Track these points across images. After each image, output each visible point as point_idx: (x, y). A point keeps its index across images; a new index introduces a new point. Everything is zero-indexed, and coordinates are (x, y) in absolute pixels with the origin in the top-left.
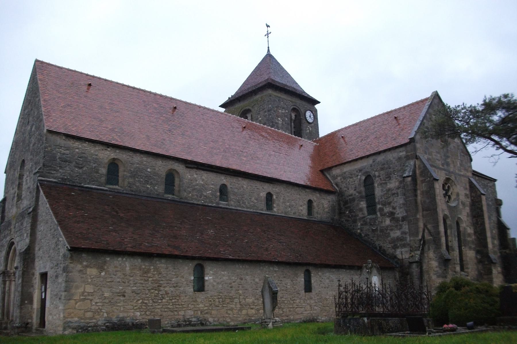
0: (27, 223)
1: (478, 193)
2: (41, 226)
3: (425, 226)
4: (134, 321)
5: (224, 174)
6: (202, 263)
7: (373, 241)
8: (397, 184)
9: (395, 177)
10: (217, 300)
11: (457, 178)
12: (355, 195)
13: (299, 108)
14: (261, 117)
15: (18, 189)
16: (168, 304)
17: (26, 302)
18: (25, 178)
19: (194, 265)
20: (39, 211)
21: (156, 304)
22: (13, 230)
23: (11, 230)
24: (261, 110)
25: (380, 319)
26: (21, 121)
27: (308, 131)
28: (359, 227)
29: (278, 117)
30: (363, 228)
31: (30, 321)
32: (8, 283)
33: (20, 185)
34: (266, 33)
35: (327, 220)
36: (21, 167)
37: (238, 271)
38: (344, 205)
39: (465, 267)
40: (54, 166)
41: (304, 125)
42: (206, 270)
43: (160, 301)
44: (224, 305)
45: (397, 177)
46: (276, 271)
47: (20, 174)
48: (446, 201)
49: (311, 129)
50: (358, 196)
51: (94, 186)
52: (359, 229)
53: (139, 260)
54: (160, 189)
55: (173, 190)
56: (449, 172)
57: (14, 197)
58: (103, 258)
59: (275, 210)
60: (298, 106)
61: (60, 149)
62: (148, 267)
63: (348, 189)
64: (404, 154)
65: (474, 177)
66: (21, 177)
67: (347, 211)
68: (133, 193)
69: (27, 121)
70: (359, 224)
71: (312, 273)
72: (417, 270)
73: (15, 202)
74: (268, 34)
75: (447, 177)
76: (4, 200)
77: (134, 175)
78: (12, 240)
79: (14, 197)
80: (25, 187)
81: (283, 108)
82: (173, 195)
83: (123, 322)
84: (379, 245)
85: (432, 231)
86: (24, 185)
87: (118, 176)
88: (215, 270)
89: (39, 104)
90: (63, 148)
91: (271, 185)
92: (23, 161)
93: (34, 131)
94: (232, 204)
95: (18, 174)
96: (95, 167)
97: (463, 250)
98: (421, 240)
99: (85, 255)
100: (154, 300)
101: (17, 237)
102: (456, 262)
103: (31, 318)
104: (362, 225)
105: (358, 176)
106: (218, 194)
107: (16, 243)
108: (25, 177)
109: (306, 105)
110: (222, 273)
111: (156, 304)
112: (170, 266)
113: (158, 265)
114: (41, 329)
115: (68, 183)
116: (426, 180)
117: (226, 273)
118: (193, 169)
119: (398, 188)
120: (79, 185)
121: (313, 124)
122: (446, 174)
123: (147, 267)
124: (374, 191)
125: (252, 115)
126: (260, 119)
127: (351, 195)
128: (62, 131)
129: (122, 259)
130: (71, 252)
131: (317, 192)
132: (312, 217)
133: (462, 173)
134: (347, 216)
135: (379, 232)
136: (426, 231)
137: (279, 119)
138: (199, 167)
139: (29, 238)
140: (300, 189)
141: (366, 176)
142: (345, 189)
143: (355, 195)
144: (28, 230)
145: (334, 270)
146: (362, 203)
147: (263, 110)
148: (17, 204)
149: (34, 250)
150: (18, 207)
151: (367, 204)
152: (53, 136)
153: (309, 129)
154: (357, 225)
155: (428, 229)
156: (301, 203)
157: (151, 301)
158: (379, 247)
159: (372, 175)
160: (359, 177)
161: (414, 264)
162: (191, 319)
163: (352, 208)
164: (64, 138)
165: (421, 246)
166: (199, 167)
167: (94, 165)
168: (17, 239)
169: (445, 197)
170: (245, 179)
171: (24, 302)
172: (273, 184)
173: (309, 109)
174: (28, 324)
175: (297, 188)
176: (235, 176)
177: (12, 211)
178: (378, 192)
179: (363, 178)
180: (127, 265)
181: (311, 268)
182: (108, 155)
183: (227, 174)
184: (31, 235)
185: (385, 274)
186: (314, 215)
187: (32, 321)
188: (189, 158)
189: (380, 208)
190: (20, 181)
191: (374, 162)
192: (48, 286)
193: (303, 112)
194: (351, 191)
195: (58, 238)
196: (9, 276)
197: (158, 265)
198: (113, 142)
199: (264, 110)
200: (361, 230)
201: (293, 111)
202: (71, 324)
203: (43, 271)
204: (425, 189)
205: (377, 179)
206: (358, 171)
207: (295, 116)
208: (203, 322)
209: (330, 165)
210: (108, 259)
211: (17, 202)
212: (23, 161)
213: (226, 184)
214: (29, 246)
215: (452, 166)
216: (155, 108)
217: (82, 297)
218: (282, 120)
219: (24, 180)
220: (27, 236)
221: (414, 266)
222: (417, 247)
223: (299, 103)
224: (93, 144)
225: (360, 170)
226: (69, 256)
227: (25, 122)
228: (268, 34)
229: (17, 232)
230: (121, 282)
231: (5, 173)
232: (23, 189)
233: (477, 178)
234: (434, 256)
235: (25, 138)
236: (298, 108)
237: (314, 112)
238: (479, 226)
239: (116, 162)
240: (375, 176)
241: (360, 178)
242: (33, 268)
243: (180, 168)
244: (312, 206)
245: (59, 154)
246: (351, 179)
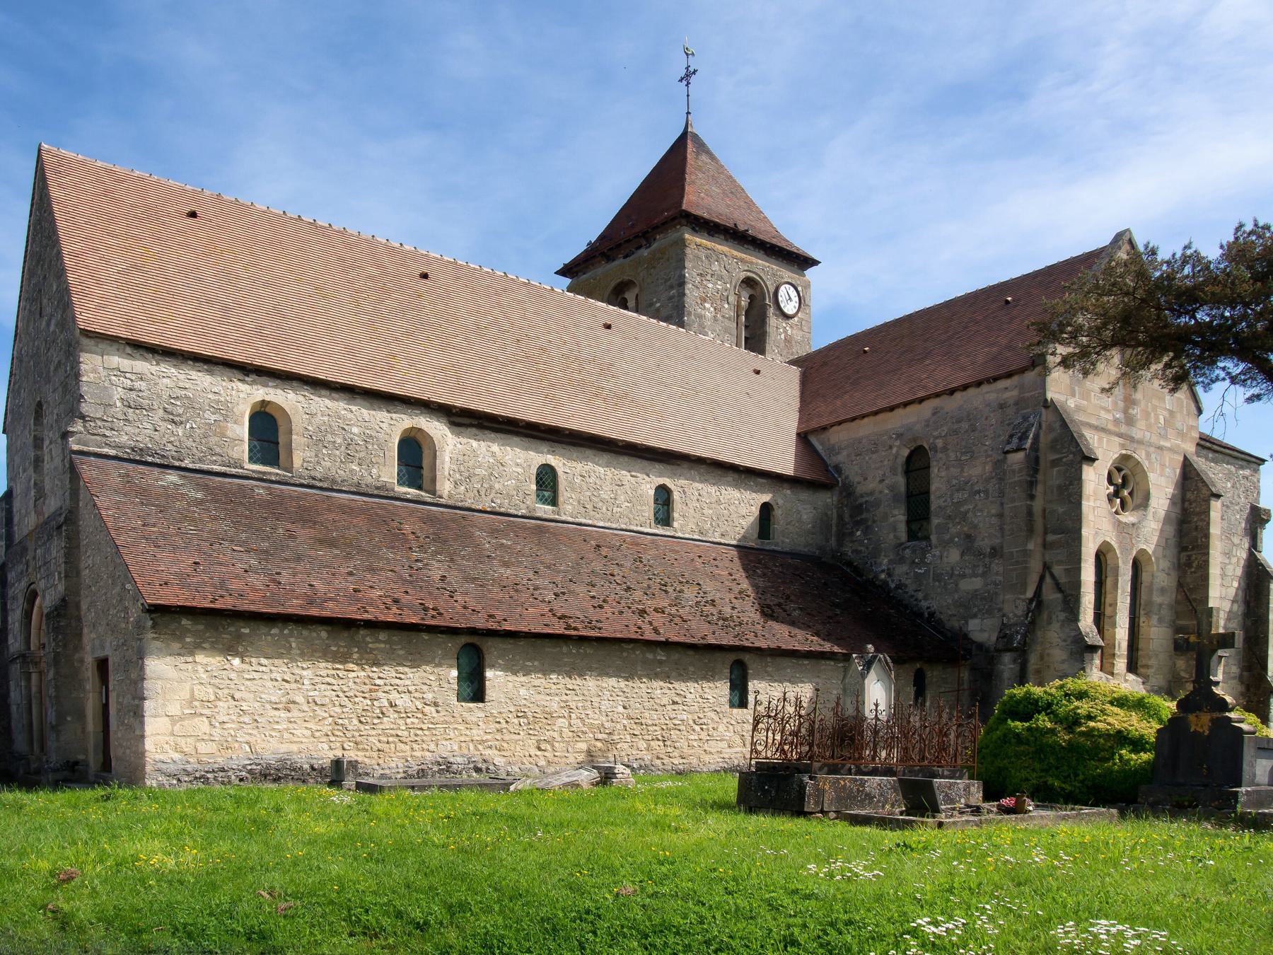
0: (56, 549)
1: (1204, 491)
2: (89, 556)
3: (1047, 567)
4: (314, 761)
5: (548, 440)
6: (478, 643)
7: (916, 600)
8: (988, 468)
9: (986, 451)
10: (516, 721)
11: (1153, 456)
12: (881, 492)
13: (761, 278)
14: (659, 300)
15: (35, 472)
16: (395, 726)
17: (69, 719)
18: (47, 448)
19: (458, 647)
20: (81, 522)
21: (366, 727)
22: (32, 563)
23: (27, 564)
24: (660, 281)
25: (841, 779)
26: (25, 306)
27: (783, 336)
28: (884, 567)
29: (705, 301)
30: (894, 569)
31: (81, 757)
32: (34, 677)
33: (38, 462)
34: (693, 79)
35: (806, 550)
36: (36, 419)
37: (566, 660)
38: (851, 516)
39: (1139, 664)
40: (110, 419)
41: (773, 321)
42: (486, 656)
43: (376, 721)
44: (531, 732)
45: (990, 453)
46: (661, 662)
47: (35, 436)
48: (1114, 510)
49: (789, 332)
50: (887, 494)
51: (215, 467)
52: (883, 571)
53: (324, 634)
54: (388, 473)
55: (421, 477)
56: (1132, 439)
57: (28, 489)
58: (232, 629)
59: (675, 524)
60: (756, 270)
61: (121, 376)
62: (346, 650)
63: (865, 479)
64: (1012, 395)
65: (1205, 452)
66: (38, 442)
67: (857, 530)
68: (319, 484)
69: (39, 309)
70: (885, 561)
71: (750, 667)
72: (1012, 666)
73: (32, 502)
74: (688, 76)
75: (1124, 452)
76: (9, 494)
77: (318, 441)
78: (32, 587)
79: (28, 489)
80: (47, 466)
81: (721, 278)
82: (420, 488)
83: (289, 762)
84: (928, 608)
85: (1063, 579)
86: (46, 462)
87: (278, 443)
88: (511, 657)
89: (59, 263)
90: (127, 375)
91: (668, 467)
92: (40, 405)
93: (54, 332)
94: (569, 508)
95: (30, 435)
96: (215, 421)
97: (1141, 624)
98: (1031, 600)
99: (189, 622)
100: (362, 719)
101: (40, 580)
102: (1119, 650)
103: (85, 751)
104: (890, 561)
105: (891, 447)
106: (534, 487)
107: (40, 593)
108: (47, 443)
109: (786, 274)
110: (527, 663)
111: (366, 727)
112: (400, 647)
113: (370, 645)
114: (105, 774)
115: (150, 459)
116: (1064, 460)
117: (536, 663)
118: (469, 429)
119: (988, 480)
120: (177, 464)
121: (796, 319)
122: (1123, 446)
123: (342, 650)
124: (929, 483)
125: (637, 295)
126: (658, 305)
127: (872, 493)
128: (124, 334)
129: (282, 631)
130: (153, 616)
131: (786, 485)
132: (768, 544)
133: (1168, 444)
134: (856, 541)
135: (931, 579)
136: (1048, 579)
137: (707, 305)
138: (486, 424)
139: (63, 582)
140: (743, 477)
141: (913, 448)
142: (857, 479)
143: (881, 492)
144: (59, 565)
145: (806, 662)
146: (896, 512)
147: (666, 281)
148: (35, 506)
149: (78, 606)
150: (39, 513)
151: (909, 515)
152: (100, 346)
153: (785, 331)
154: (881, 564)
155: (1052, 575)
156: (743, 511)
157: (355, 722)
158: (929, 614)
159: (927, 447)
160: (894, 450)
161: (1008, 654)
162: (452, 760)
163: (870, 523)
164: (128, 350)
165: (1030, 614)
166: (486, 424)
167: (213, 417)
168: (42, 584)
169: (1110, 500)
170: (601, 453)
171: (66, 719)
172: (673, 464)
173: (790, 281)
174: (76, 763)
175: (736, 476)
176: (574, 445)
177: (26, 522)
178: (938, 484)
179: (906, 452)
180: (294, 645)
181: (746, 658)
182: (247, 395)
183: (554, 441)
184: (66, 577)
185: (935, 673)
186: (774, 538)
187: (87, 756)
188: (459, 402)
189: (939, 524)
190: (39, 453)
191: (934, 414)
192: (111, 688)
193: (772, 290)
194: (871, 485)
195: (123, 585)
196: (36, 664)
197: (370, 645)
198: (259, 362)
199: (668, 283)
200: (889, 575)
201: (744, 286)
202: (164, 766)
203: (100, 654)
204: (1058, 482)
205: (940, 455)
206: (894, 436)
207: (750, 297)
208: (480, 765)
209: (824, 422)
210: (247, 631)
211: (36, 501)
212: (40, 405)
213: (553, 464)
214: (63, 600)
215: (1141, 424)
216: (371, 278)
217: (187, 711)
218: (715, 309)
219: (46, 450)
220: (60, 578)
221: (1007, 658)
222: (1020, 617)
223: (763, 267)
224: (205, 367)
225: (899, 436)
226: (150, 623)
227: (33, 309)
228: (688, 76)
229: (40, 567)
230: (280, 679)
231: (4, 432)
232: (46, 471)
233: (1210, 455)
234: (1060, 638)
235: (38, 348)
236: (758, 278)
237: (800, 289)
238: (1193, 570)
239: (268, 410)
240: (934, 449)
241: (897, 451)
242: (79, 647)
243: (436, 428)
244: (772, 518)
245: (119, 389)
246: (874, 456)
